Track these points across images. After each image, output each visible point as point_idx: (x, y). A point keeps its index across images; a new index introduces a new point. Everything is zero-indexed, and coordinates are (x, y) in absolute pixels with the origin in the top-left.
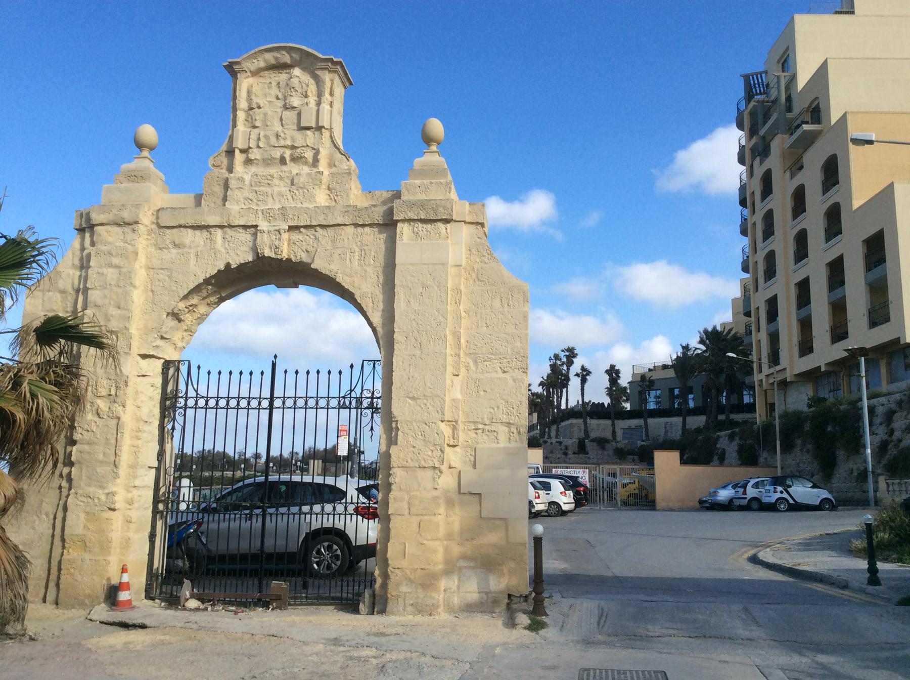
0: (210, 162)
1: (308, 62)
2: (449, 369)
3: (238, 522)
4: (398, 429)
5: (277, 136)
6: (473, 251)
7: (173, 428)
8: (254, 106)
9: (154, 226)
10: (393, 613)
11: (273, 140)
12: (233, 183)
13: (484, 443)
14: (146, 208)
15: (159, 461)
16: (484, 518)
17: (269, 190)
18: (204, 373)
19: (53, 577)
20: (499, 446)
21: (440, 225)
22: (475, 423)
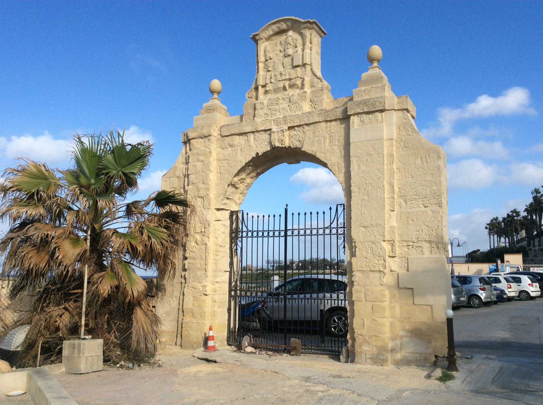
0: (247, 96)
1: (296, 26)
2: (387, 208)
4: (356, 247)
5: (281, 74)
7: (237, 249)
8: (268, 58)
9: (220, 137)
10: (358, 363)
11: (279, 78)
12: (258, 106)
13: (413, 254)
14: (215, 127)
17: (277, 107)
19: (179, 331)
20: (423, 256)
21: (378, 114)
22: (406, 241)
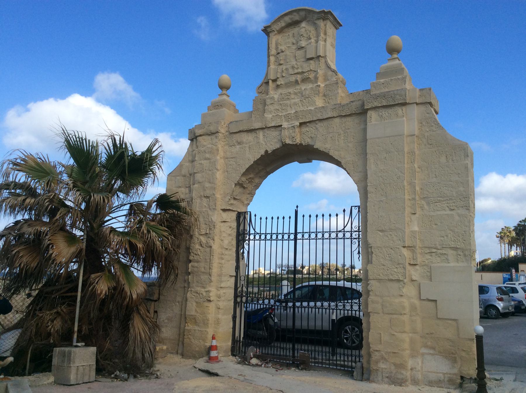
2: (408, 210)
3: (279, 311)
4: (372, 253)
6: (424, 123)
7: (243, 252)
10: (374, 382)
12: (268, 102)
14: (223, 123)
15: (237, 273)
16: (440, 319)
18: (258, 218)
